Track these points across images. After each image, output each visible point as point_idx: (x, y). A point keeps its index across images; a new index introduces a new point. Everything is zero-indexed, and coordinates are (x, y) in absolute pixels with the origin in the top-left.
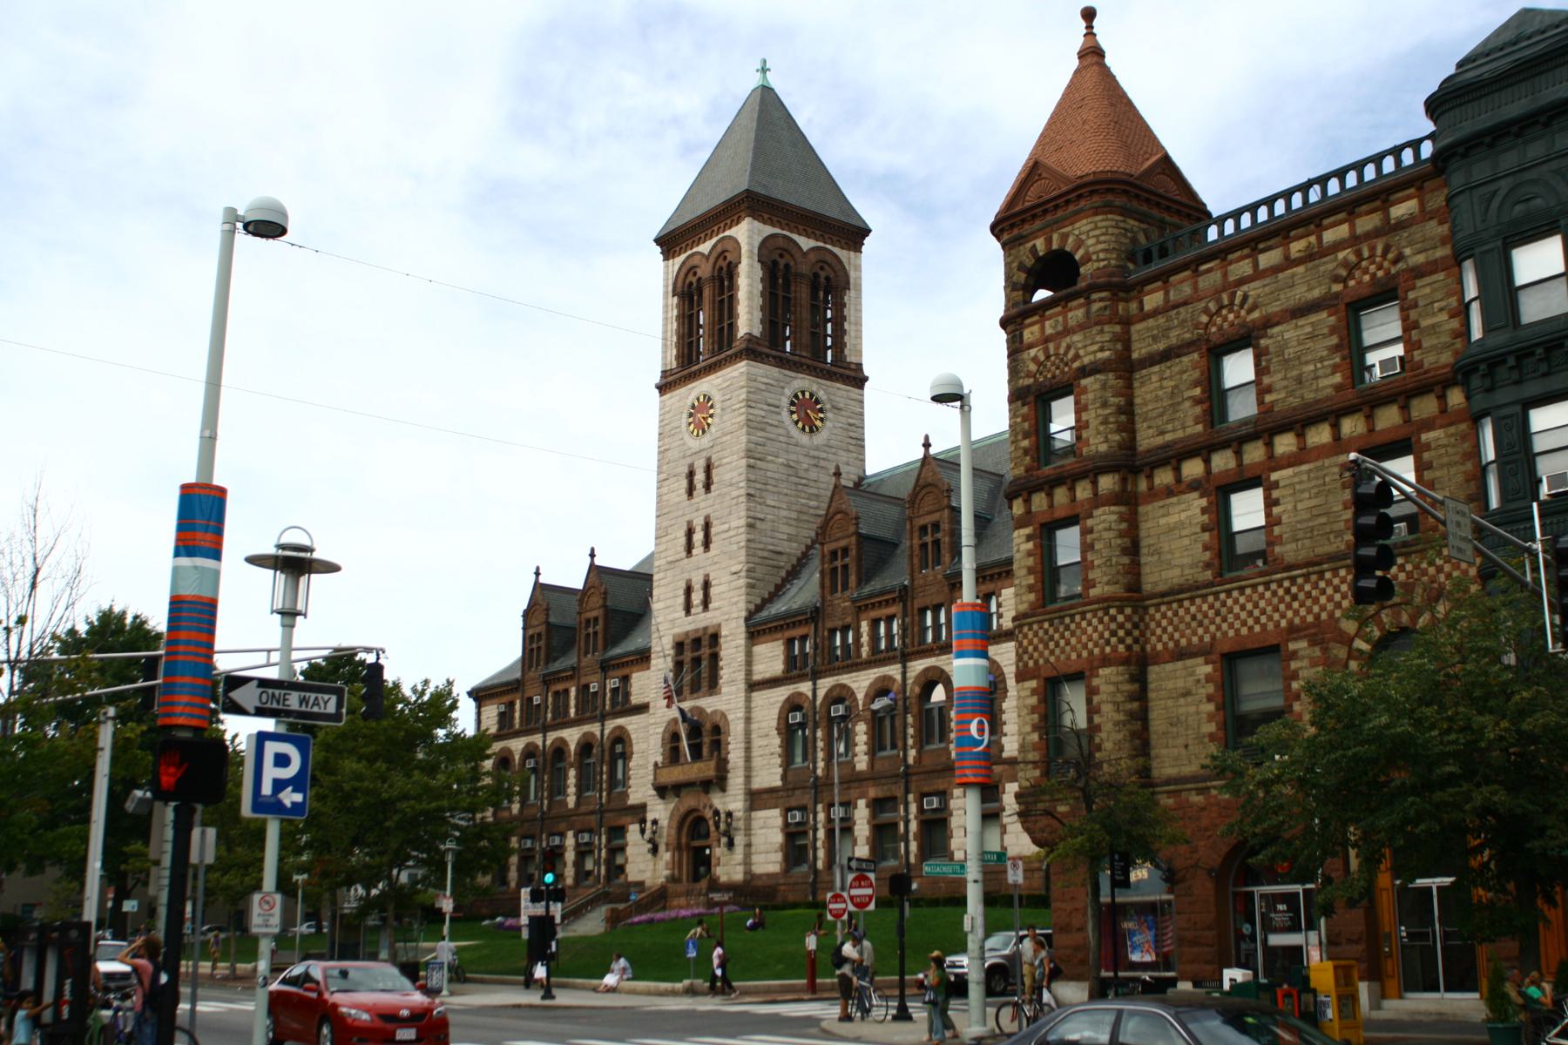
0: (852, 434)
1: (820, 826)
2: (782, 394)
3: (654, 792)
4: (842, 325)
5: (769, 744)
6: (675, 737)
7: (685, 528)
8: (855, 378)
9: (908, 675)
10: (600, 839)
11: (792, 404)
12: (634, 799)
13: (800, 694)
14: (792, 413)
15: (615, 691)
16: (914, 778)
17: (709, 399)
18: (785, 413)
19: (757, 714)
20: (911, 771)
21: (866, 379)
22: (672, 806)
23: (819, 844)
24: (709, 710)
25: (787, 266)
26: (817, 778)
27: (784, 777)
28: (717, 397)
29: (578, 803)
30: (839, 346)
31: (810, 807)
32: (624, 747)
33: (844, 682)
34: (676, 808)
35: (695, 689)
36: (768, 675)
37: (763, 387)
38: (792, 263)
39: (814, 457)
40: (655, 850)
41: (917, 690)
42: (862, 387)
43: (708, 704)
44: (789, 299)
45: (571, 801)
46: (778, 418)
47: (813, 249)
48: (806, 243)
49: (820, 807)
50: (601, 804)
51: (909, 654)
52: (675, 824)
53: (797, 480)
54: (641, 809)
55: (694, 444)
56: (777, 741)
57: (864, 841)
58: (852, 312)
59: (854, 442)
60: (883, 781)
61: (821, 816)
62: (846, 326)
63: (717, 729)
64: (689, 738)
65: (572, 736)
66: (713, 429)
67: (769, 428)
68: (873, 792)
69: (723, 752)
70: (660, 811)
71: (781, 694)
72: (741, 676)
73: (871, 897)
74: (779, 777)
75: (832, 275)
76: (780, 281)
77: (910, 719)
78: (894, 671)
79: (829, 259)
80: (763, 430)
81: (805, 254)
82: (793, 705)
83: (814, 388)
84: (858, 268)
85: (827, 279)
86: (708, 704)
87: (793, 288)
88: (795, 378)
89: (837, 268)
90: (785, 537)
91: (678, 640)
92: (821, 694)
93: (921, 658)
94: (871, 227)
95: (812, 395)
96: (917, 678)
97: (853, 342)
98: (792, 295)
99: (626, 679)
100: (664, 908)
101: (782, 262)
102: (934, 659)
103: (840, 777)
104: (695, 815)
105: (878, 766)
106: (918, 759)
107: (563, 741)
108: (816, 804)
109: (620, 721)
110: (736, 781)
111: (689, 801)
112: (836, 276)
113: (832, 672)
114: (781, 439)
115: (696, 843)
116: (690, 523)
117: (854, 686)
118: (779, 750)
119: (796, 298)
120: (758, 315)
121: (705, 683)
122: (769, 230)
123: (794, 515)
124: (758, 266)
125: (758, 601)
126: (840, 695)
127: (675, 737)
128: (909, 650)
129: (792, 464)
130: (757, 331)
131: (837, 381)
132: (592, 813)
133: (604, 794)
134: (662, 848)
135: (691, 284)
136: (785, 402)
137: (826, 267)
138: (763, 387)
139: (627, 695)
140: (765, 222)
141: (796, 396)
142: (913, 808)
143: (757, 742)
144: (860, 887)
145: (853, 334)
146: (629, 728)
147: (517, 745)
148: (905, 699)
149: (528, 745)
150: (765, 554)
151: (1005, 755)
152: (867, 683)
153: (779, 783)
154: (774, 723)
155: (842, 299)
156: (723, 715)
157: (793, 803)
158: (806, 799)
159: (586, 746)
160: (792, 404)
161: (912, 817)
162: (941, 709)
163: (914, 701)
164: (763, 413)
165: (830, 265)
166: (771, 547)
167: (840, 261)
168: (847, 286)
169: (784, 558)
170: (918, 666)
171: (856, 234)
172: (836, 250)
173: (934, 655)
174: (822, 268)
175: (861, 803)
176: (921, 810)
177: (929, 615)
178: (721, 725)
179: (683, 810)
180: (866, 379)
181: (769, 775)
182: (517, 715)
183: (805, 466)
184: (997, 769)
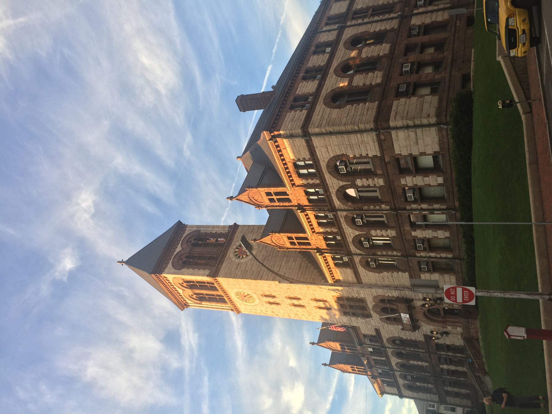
0: (256, 231)
1: (428, 255)
2: (234, 261)
3: (417, 331)
4: (213, 234)
5: (386, 277)
6: (388, 319)
7: (293, 307)
8: (234, 229)
9: (343, 208)
10: (443, 355)
11: (239, 257)
12: (422, 339)
13: (360, 261)
14: (243, 257)
15: (370, 340)
16: (397, 205)
17: (237, 293)
18: (242, 261)
19: (373, 281)
20: (393, 207)
21: (235, 224)
22: (423, 324)
23: (438, 256)
24: (374, 304)
25: (186, 257)
26: (402, 256)
27: (404, 271)
28: (235, 290)
29: (426, 361)
30: (221, 235)
31: (418, 259)
32: (397, 340)
33: (351, 240)
34: (424, 322)
35: (365, 308)
36: (354, 276)
37: (229, 270)
38: (185, 255)
39: (262, 248)
40: (447, 333)
41: (350, 204)
42: (238, 226)
43: (370, 304)
44: (199, 256)
45: (425, 364)
46: (243, 264)
47: (182, 246)
48: (179, 249)
49: (418, 255)
50: (425, 352)
51: (332, 208)
52: (433, 323)
53: (271, 256)
54: (426, 336)
55: (257, 301)
56: (385, 273)
57: (436, 233)
58: (209, 229)
59: (259, 230)
60: (400, 222)
61: (423, 254)
62: (214, 232)
63: (383, 301)
64: (389, 314)
65: (394, 361)
66: (249, 293)
67: (247, 269)
68: (407, 228)
69: (393, 299)
70: (426, 328)
71: (361, 270)
72: (355, 289)
73: (463, 290)
74: (403, 274)
75: (194, 238)
76: (191, 260)
77: (366, 208)
78: (341, 215)
79: (187, 238)
80: (247, 271)
81: (183, 249)
82: (367, 265)
83: (235, 247)
84: (192, 226)
85: (195, 240)
86: (370, 304)
87: (195, 255)
88: (229, 255)
89: (189, 236)
90: (294, 263)
91: (343, 314)
92: (358, 251)
93: (333, 202)
94: (176, 221)
95: (237, 248)
96: (343, 204)
97: (220, 229)
98: (198, 255)
99: (365, 336)
100: (477, 340)
101: (184, 259)
102: (333, 195)
103: (422, 221)
104: (427, 313)
105: (393, 225)
106: (386, 203)
107: (396, 364)
108: (416, 256)
109: (385, 340)
110: (408, 294)
111: (419, 316)
112: (193, 236)
113: (347, 246)
114: (252, 263)
115: (442, 312)
116: (290, 305)
117: (352, 236)
118: (390, 273)
119: (199, 254)
120: (202, 271)
121: (361, 304)
122: (170, 265)
123: (285, 258)
124: (183, 270)
125: (320, 278)
126: (358, 242)
127: (388, 319)
128: (329, 207)
129: (263, 259)
130: (207, 272)
131: (233, 236)
132: (430, 356)
133: (420, 350)
134: (445, 330)
135: (196, 297)
136: (237, 261)
137: (190, 240)
138: (229, 270)
139: (372, 336)
140: (167, 267)
141: (236, 255)
142: (414, 206)
143: (387, 282)
144: (455, 295)
145: (217, 229)
146: (387, 337)
147: (401, 382)
148: (355, 210)
149: (400, 377)
150: (300, 273)
151: (379, 155)
152: (350, 229)
153: (407, 273)
154: (377, 274)
155: (203, 233)
156: (375, 297)
157: (417, 267)
158: (414, 261)
159: (399, 355)
160: (239, 257)
161: (419, 207)
162: (359, 191)
163: (356, 206)
164: (240, 272)
165: (190, 238)
166: (297, 270)
167: (189, 234)
168: (198, 231)
169: (303, 264)
170: (337, 203)
171: (180, 226)
172: (184, 236)
173: (330, 194)
174: (190, 242)
175: (414, 234)
176: (415, 202)
177: (311, 197)
178: (380, 299)
179: (424, 319)
180: (235, 224)
181: (403, 278)
182: (387, 380)
183: (265, 253)
184: (387, 159)
